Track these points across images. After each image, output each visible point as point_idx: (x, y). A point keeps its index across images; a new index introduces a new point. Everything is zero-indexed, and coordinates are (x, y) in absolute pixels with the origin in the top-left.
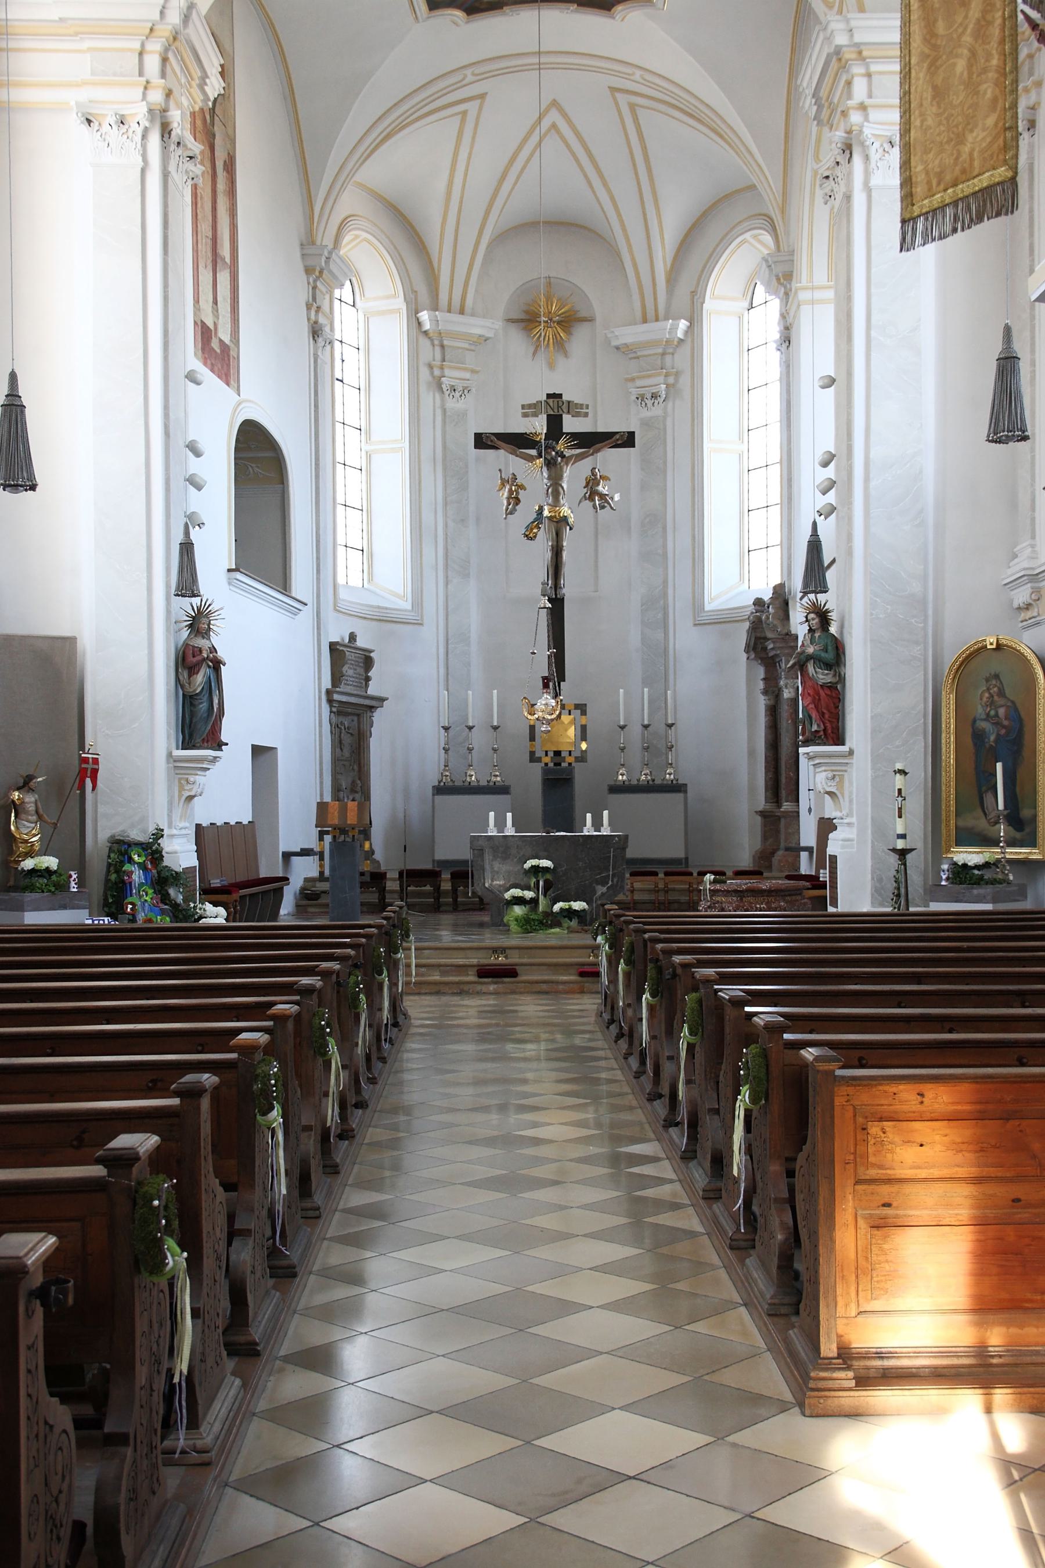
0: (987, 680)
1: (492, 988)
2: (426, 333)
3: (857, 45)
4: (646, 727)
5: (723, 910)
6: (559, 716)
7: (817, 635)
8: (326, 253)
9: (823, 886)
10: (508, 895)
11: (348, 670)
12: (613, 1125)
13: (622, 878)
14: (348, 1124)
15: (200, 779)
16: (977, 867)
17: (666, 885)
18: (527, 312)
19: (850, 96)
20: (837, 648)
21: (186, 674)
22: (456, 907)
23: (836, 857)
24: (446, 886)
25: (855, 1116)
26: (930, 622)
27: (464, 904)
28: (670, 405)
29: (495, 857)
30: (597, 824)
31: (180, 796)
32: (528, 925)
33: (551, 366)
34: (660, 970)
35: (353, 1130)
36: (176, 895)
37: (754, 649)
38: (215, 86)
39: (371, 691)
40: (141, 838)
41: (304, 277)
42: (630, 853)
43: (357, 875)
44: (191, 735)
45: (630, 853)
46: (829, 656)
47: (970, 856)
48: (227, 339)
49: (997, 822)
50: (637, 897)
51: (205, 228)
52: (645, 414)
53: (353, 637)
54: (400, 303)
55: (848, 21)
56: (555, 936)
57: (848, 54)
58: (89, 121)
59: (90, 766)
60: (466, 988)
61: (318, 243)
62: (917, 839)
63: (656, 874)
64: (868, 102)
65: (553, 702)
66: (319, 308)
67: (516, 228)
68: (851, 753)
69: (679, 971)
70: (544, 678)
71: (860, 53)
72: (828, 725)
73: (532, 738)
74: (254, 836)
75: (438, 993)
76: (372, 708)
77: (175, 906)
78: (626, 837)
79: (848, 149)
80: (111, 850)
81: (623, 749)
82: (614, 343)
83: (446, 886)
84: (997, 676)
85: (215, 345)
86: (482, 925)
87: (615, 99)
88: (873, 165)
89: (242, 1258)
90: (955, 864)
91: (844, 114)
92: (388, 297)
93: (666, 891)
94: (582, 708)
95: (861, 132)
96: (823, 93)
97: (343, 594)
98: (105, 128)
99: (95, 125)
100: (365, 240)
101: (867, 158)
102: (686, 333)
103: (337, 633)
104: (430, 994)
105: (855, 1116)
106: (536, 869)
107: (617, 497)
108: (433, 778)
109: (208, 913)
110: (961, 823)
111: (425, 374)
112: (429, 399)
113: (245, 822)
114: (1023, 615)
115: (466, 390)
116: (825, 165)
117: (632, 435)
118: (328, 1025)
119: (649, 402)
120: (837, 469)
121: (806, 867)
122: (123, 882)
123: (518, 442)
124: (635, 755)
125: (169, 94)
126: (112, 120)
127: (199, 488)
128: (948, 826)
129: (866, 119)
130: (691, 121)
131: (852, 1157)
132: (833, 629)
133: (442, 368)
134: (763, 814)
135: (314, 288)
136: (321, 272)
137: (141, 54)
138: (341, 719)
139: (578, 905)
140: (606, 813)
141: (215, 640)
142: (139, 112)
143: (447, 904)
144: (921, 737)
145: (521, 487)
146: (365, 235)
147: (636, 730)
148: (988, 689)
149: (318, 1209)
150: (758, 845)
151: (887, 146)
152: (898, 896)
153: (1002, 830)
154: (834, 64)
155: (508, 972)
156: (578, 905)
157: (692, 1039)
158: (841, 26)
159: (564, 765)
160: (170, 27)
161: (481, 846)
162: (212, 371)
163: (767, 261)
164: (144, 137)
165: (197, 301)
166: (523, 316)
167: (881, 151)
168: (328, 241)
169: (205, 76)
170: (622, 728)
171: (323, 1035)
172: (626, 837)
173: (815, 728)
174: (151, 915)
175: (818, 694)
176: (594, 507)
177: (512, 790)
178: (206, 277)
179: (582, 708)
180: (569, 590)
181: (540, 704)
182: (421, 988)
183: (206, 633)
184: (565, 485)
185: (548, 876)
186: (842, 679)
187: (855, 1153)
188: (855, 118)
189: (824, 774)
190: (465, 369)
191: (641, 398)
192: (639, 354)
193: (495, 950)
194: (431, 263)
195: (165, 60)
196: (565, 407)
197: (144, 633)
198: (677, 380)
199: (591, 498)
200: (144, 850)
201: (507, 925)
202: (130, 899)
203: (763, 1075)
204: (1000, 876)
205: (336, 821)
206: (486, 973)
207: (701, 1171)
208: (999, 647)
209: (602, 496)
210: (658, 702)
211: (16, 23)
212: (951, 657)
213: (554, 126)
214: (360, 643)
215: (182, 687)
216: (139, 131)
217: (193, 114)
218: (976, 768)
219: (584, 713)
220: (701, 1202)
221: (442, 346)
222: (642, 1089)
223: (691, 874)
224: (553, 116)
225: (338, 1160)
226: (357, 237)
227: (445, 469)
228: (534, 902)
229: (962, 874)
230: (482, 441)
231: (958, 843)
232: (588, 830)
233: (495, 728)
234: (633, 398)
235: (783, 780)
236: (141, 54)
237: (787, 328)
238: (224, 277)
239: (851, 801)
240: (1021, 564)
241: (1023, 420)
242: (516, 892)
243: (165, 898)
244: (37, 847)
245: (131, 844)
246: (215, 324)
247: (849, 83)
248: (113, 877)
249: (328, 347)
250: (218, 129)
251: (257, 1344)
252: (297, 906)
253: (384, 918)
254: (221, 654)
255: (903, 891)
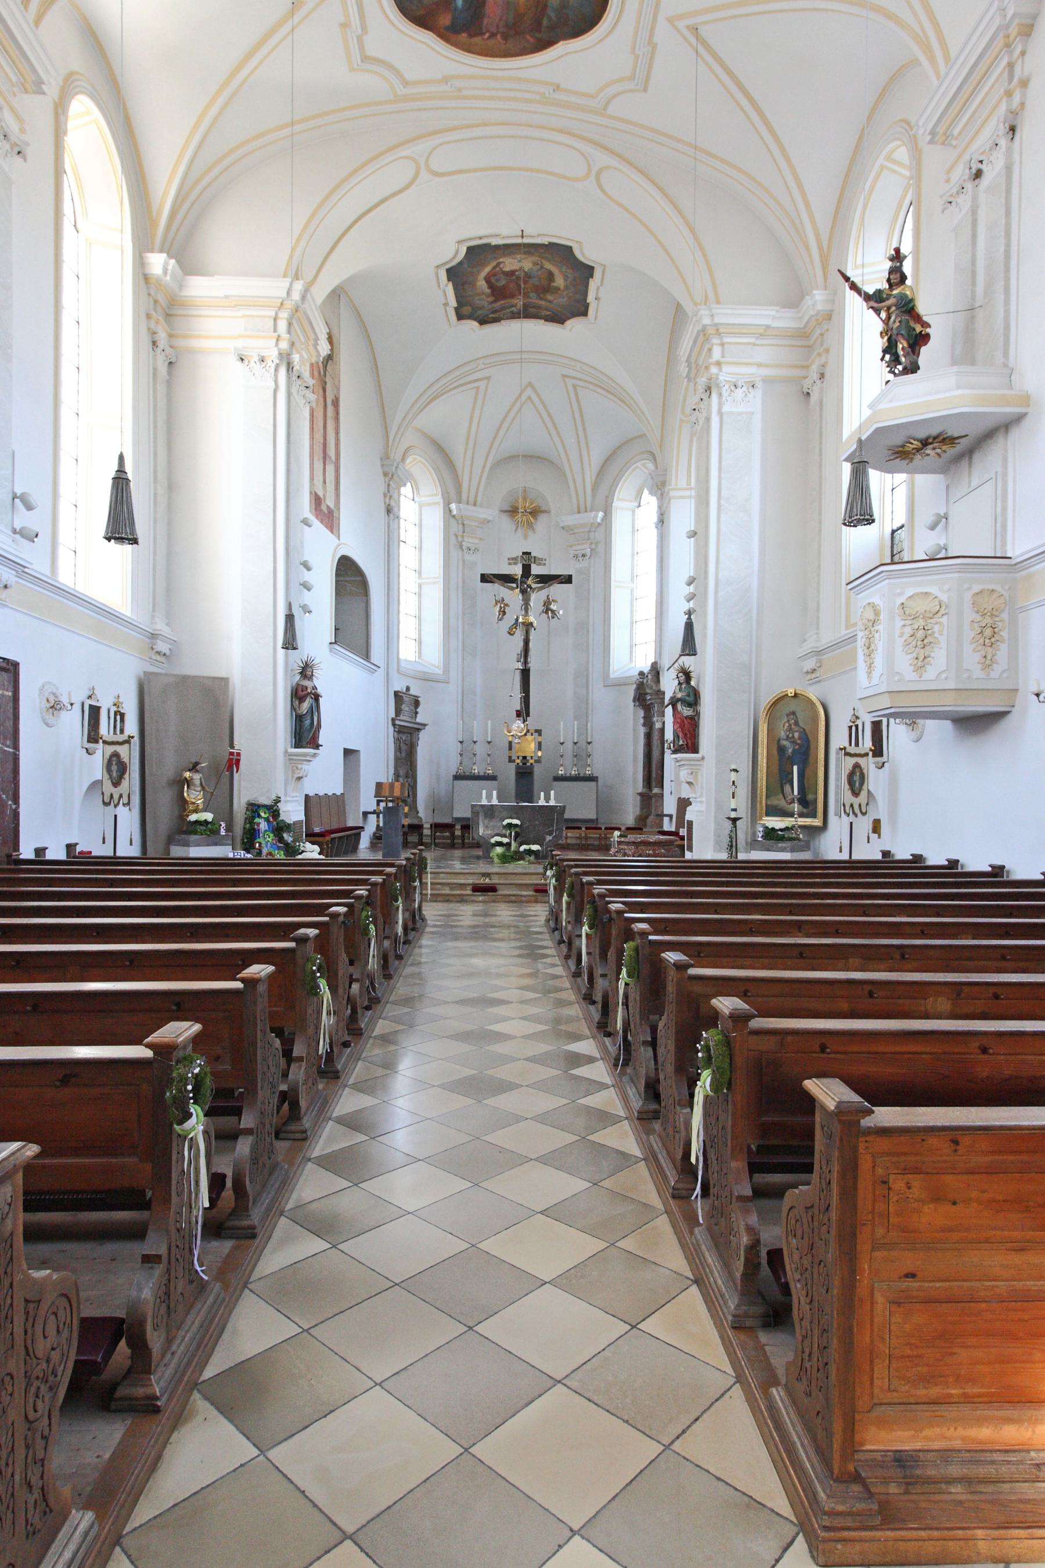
0: (787, 715)
1: (481, 898)
2: (454, 516)
3: (716, 325)
4: (575, 743)
5: (625, 855)
6: (525, 735)
7: (683, 686)
8: (395, 464)
9: (682, 838)
10: (493, 841)
11: (405, 708)
12: (558, 1021)
13: (561, 831)
14: (358, 1025)
15: (305, 766)
16: (781, 830)
17: (586, 834)
18: (512, 506)
19: (710, 357)
20: (695, 695)
21: (297, 703)
22: (463, 846)
23: (692, 822)
24: (458, 833)
25: (874, 1167)
26: (753, 679)
27: (469, 843)
28: (592, 560)
29: (485, 818)
30: (547, 799)
31: (293, 776)
32: (505, 859)
33: (526, 537)
34: (596, 910)
35: (361, 1029)
36: (288, 837)
37: (638, 700)
38: (324, 349)
39: (418, 720)
40: (268, 802)
41: (382, 478)
42: (566, 816)
43: (400, 827)
44: (300, 740)
45: (566, 816)
46: (691, 699)
47: (776, 823)
48: (332, 505)
49: (793, 802)
50: (569, 841)
51: (319, 437)
52: (579, 565)
53: (408, 689)
54: (439, 499)
55: (710, 309)
56: (520, 866)
57: (711, 331)
58: (242, 360)
59: (235, 757)
60: (465, 898)
61: (392, 458)
62: (743, 812)
63: (580, 828)
64: (722, 360)
65: (522, 726)
66: (391, 497)
67: (505, 459)
68: (703, 758)
69: (614, 916)
70: (517, 711)
71: (717, 330)
72: (689, 741)
73: (510, 748)
74: (344, 801)
75: (448, 901)
76: (419, 730)
77: (287, 844)
78: (565, 807)
79: (708, 389)
80: (247, 809)
81: (562, 756)
82: (562, 525)
83: (458, 833)
84: (794, 713)
85: (324, 508)
86: (478, 858)
87: (564, 381)
88: (724, 399)
89: (143, 1296)
90: (767, 827)
91: (707, 368)
92: (432, 495)
93: (586, 838)
94: (539, 732)
95: (717, 378)
96: (693, 360)
97: (402, 664)
98: (252, 364)
99: (246, 362)
100: (420, 461)
101: (720, 395)
102: (602, 520)
103: (399, 686)
104: (443, 901)
105: (874, 1167)
106: (510, 826)
107: (561, 612)
108: (453, 771)
109: (307, 850)
110: (769, 803)
111: (453, 540)
112: (455, 553)
113: (338, 793)
114: (809, 676)
115: (476, 550)
116: (692, 401)
117: (570, 576)
118: (319, 970)
119: (581, 559)
120: (696, 588)
121: (668, 826)
122: (254, 829)
123: (506, 579)
124: (569, 760)
125: (293, 344)
126: (256, 359)
127: (309, 590)
128: (761, 803)
129: (721, 370)
130: (609, 396)
131: (870, 1217)
132: (693, 683)
133: (463, 537)
134: (641, 794)
135: (389, 485)
136: (392, 476)
137: (275, 319)
138: (400, 735)
139: (535, 847)
140: (552, 792)
141: (316, 682)
142: (273, 354)
143: (458, 843)
144: (745, 750)
145: (507, 605)
146: (420, 458)
147: (569, 745)
148: (788, 721)
149: (305, 1132)
150: (638, 812)
151: (733, 388)
152: (731, 846)
153: (796, 807)
154: (701, 338)
155: (492, 889)
156: (535, 847)
157: (628, 980)
158: (707, 312)
159: (528, 764)
160: (293, 302)
161: (477, 810)
162: (322, 522)
163: (651, 475)
164: (276, 370)
165: (312, 479)
166: (510, 509)
167: (729, 390)
168: (398, 457)
169: (316, 339)
170: (562, 744)
171: (315, 979)
172: (565, 807)
173: (681, 743)
174: (271, 850)
175: (683, 722)
176: (548, 617)
177: (498, 778)
178: (318, 466)
179: (539, 732)
180: (533, 665)
181: (514, 727)
182: (436, 898)
183: (310, 678)
184: (532, 604)
185: (517, 829)
186: (698, 714)
187: (873, 1212)
188: (714, 370)
189: (686, 771)
190: (476, 538)
191: (576, 556)
192: (576, 531)
193: (484, 875)
194: (457, 476)
195: (290, 324)
196: (533, 560)
197: (271, 676)
198: (596, 546)
199: (546, 612)
200: (268, 809)
201: (492, 858)
202: (258, 840)
203: (726, 1065)
204: (794, 836)
205: (387, 794)
206: (477, 889)
207: (634, 1089)
208: (796, 695)
209: (553, 611)
210: (583, 729)
211: (198, 299)
212: (766, 700)
213: (529, 398)
214: (412, 692)
215: (295, 710)
216: (273, 366)
217: (312, 365)
218: (780, 770)
219: (540, 735)
220: (635, 1121)
221: (463, 525)
222: (579, 989)
223: (601, 829)
224: (529, 392)
225: (339, 1067)
226: (415, 459)
227: (463, 595)
228: (509, 845)
229: (771, 834)
230: (485, 578)
231: (767, 815)
232: (542, 802)
233: (489, 743)
234: (572, 556)
235: (654, 775)
236: (275, 319)
237: (662, 514)
238: (330, 469)
239: (702, 788)
240: (809, 645)
241: (871, 508)
242: (498, 839)
243: (281, 839)
244: (201, 807)
245: (259, 806)
246: (324, 495)
247: (710, 350)
248: (248, 826)
249: (396, 520)
250: (328, 379)
251: (157, 1398)
252: (371, 843)
253: (412, 854)
254: (320, 691)
255: (734, 844)
